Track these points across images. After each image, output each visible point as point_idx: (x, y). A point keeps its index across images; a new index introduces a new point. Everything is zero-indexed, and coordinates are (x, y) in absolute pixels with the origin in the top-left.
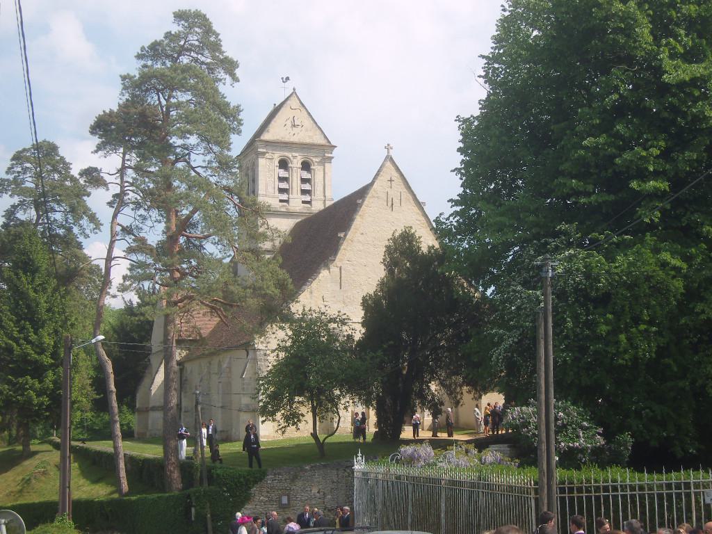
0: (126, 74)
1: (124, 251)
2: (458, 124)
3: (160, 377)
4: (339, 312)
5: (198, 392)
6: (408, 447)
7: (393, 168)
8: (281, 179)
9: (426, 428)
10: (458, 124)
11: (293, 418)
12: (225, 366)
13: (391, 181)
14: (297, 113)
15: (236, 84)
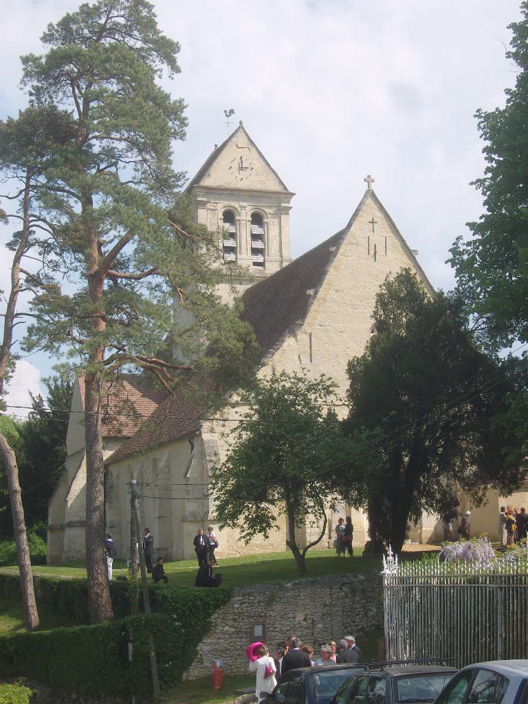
0: (28, 54)
1: (30, 303)
2: (478, 120)
3: (80, 482)
4: (323, 375)
5: (135, 482)
6: (456, 543)
7: (375, 206)
9: (425, 541)
10: (478, 120)
11: (261, 523)
12: (162, 464)
13: (372, 223)
14: (245, 153)
15: (176, 76)
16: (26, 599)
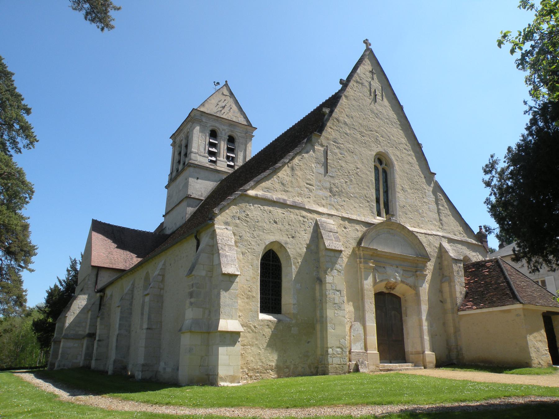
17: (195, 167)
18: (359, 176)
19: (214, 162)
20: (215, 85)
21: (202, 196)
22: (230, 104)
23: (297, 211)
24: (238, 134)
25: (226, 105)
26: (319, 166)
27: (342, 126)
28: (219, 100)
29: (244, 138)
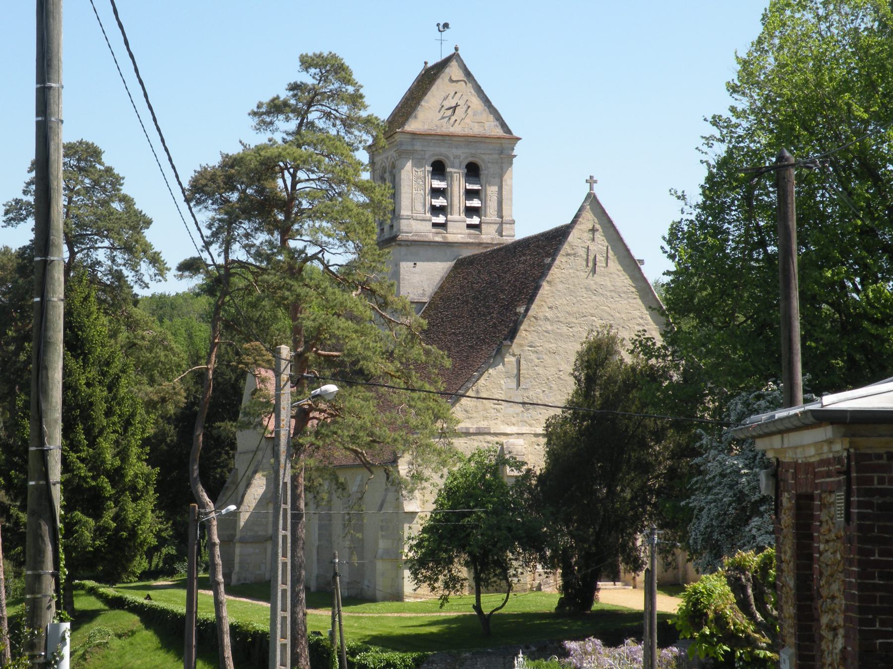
8: (436, 192)
16: (223, 652)
17: (407, 245)
18: (562, 379)
19: (443, 226)
20: (439, 31)
21: (424, 295)
22: (465, 98)
23: (481, 437)
24: (485, 159)
25: (457, 105)
26: (509, 380)
27: (541, 323)
28: (444, 95)
29: (497, 163)
